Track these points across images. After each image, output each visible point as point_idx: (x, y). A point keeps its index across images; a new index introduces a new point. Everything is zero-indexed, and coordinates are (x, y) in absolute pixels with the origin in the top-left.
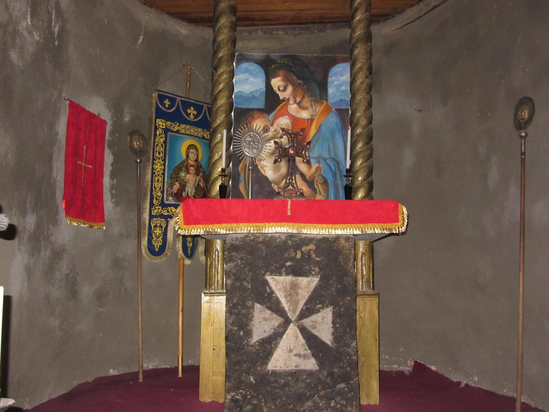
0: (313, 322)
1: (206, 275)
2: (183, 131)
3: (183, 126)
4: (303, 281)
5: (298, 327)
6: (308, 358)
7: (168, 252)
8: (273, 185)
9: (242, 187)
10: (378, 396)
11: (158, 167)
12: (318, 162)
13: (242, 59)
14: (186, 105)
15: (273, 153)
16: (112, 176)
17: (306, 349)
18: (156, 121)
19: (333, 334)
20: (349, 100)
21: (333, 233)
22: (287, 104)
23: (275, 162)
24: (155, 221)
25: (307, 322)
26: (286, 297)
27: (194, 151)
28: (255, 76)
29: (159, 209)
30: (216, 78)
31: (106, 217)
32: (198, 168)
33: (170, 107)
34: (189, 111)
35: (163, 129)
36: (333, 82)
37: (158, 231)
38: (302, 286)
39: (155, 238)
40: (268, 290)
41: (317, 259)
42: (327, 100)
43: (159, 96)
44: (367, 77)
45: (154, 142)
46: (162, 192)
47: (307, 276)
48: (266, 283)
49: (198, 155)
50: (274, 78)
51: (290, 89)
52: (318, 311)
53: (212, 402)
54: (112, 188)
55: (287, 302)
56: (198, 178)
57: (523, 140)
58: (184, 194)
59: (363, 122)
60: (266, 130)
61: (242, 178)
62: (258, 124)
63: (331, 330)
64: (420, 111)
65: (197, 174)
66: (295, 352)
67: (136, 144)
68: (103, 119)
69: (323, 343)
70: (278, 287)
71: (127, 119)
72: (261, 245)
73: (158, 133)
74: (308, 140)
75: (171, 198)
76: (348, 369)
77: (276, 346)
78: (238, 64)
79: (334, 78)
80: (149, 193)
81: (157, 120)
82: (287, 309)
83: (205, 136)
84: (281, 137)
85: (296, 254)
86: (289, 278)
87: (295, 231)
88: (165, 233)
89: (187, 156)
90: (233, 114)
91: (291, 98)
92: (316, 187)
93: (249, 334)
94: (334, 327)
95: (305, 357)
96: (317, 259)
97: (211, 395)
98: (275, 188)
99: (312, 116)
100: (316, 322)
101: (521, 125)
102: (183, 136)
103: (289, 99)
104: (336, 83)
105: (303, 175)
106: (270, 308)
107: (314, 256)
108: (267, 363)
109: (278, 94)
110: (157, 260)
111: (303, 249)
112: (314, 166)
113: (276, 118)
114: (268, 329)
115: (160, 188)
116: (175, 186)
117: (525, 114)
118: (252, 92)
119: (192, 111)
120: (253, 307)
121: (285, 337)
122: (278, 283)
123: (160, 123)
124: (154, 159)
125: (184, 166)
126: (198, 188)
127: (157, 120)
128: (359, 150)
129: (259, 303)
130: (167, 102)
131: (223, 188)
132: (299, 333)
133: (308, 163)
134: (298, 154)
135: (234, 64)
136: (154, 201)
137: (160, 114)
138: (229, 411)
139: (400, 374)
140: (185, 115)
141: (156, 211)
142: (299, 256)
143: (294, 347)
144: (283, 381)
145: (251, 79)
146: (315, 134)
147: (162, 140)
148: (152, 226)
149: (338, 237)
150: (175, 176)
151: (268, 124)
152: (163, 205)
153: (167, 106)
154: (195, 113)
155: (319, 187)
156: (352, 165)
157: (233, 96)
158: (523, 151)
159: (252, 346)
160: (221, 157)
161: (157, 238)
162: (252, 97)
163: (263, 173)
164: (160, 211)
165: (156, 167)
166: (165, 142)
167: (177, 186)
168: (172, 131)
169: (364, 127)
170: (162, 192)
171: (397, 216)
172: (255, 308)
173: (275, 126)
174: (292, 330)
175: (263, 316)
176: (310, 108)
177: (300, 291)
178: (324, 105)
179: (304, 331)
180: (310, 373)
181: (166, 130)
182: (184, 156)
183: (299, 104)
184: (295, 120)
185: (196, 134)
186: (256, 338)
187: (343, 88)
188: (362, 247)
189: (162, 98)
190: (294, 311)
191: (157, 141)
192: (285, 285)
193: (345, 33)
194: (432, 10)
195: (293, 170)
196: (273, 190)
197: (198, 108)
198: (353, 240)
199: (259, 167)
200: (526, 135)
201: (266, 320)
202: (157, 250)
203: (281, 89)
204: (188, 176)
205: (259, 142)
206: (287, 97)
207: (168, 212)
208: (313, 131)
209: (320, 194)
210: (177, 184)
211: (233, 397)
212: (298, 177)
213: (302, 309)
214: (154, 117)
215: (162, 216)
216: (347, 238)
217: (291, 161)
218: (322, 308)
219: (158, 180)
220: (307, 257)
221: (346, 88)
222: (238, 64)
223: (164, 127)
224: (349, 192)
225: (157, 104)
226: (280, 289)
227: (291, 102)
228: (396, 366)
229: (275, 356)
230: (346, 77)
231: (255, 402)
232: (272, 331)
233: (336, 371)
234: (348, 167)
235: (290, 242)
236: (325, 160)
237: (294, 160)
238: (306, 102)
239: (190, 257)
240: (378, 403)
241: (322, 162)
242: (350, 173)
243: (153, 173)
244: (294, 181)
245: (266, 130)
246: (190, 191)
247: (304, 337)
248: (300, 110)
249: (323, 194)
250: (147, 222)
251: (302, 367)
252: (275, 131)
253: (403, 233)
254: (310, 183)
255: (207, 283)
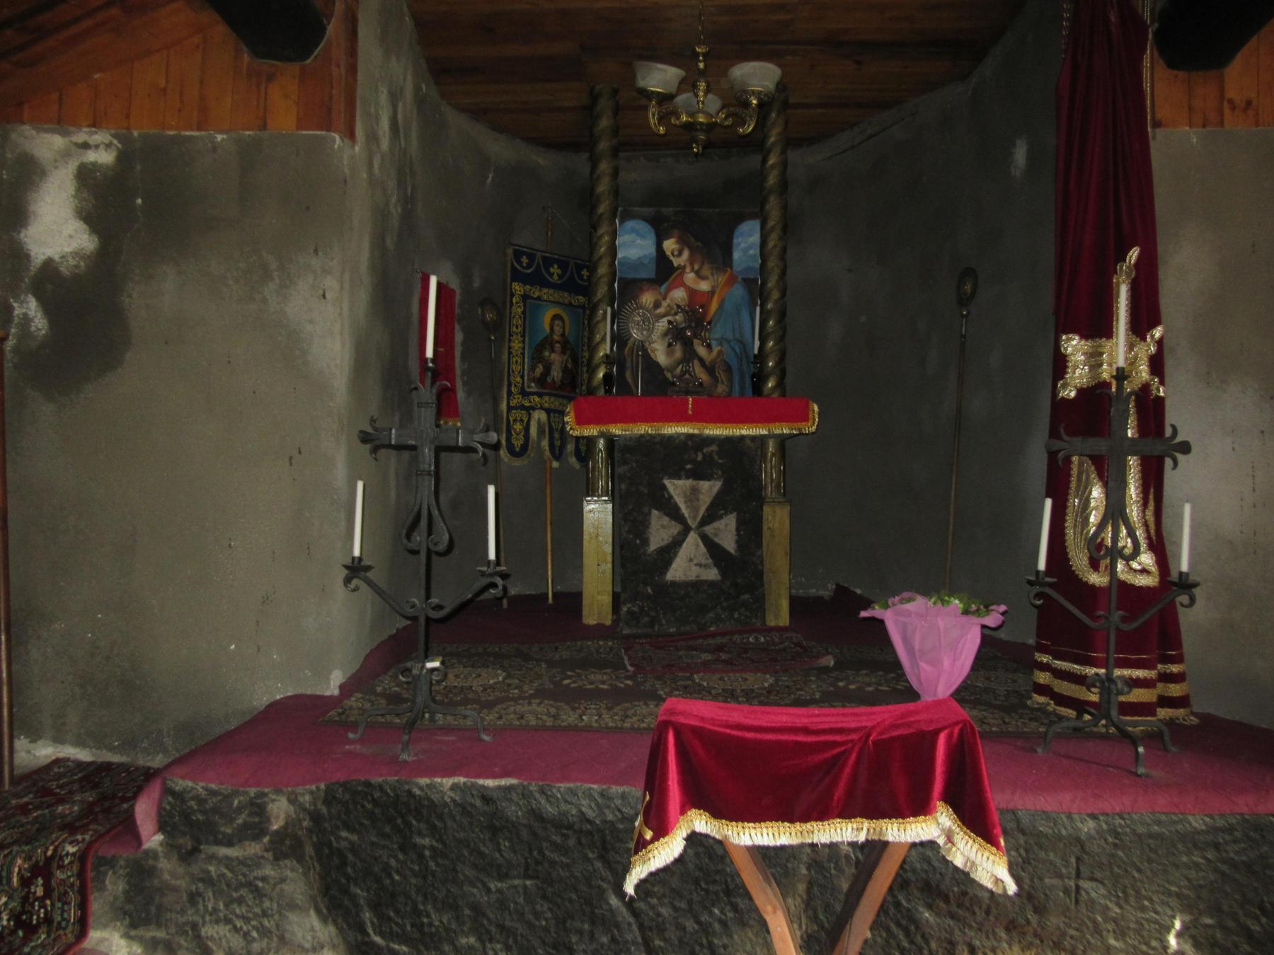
0: (715, 529)
1: (588, 479)
2: (545, 297)
3: (545, 290)
4: (704, 485)
5: (699, 535)
6: (710, 568)
7: (531, 453)
8: (665, 372)
9: (628, 375)
10: (787, 616)
11: (516, 345)
12: (721, 344)
13: (627, 216)
14: (548, 262)
15: (665, 334)
16: (463, 358)
17: (707, 558)
18: (511, 285)
19: (737, 542)
20: (758, 266)
21: (738, 434)
22: (682, 274)
23: (670, 345)
24: (516, 414)
25: (708, 529)
26: (685, 502)
27: (560, 323)
28: (643, 237)
29: (518, 398)
30: (595, 240)
31: (461, 408)
32: (565, 344)
33: (529, 266)
34: (552, 270)
35: (521, 295)
36: (739, 244)
37: (518, 427)
38: (703, 491)
39: (514, 435)
40: (666, 496)
41: (720, 461)
42: (731, 268)
43: (515, 251)
44: (780, 239)
45: (511, 313)
46: (522, 377)
47: (709, 480)
48: (664, 488)
49: (564, 328)
50: (667, 239)
51: (686, 254)
52: (720, 517)
53: (598, 624)
54: (463, 374)
55: (687, 507)
56: (565, 357)
57: (964, 320)
58: (549, 380)
59: (775, 295)
60: (657, 305)
61: (628, 364)
62: (647, 298)
63: (735, 538)
64: (850, 271)
65: (563, 352)
66: (695, 562)
67: (489, 316)
68: (452, 287)
69: (724, 551)
70: (677, 492)
71: (477, 284)
72: (658, 447)
73: (514, 300)
74: (708, 320)
75: (533, 385)
76: (753, 579)
77: (675, 555)
78: (622, 222)
79: (740, 239)
80: (506, 378)
81: (513, 284)
82: (686, 515)
83: (573, 302)
84: (676, 314)
85: (697, 456)
86: (688, 483)
87: (696, 432)
88: (527, 429)
89: (552, 329)
90: (616, 285)
91: (688, 264)
92: (717, 374)
93: (646, 542)
94: (738, 534)
95: (706, 566)
96: (720, 461)
97: (596, 617)
98: (669, 375)
99: (713, 287)
100: (718, 529)
101: (964, 301)
102: (544, 303)
103: (684, 267)
104: (743, 245)
105: (701, 360)
106: (667, 515)
107: (716, 457)
108: (665, 574)
109: (671, 261)
110: (517, 463)
111: (705, 450)
112: (716, 349)
113: (669, 290)
114: (666, 538)
115: (519, 372)
116: (538, 370)
117: (968, 288)
118: (639, 258)
119: (555, 270)
120: (649, 513)
121: (684, 545)
122: (676, 487)
123: (517, 288)
124: (511, 335)
125: (547, 343)
126: (565, 370)
127: (513, 284)
128: (770, 330)
129: (657, 509)
130: (525, 260)
131: (607, 377)
132: (700, 541)
133: (709, 347)
134: (695, 335)
135: (617, 221)
136: (513, 389)
137: (517, 276)
138: (415, 953)
139: (819, 599)
140: (548, 277)
141: (515, 401)
142: (700, 457)
143: (695, 556)
144: (682, 592)
145: (639, 241)
146: (717, 310)
147: (520, 310)
148: (511, 419)
149: (742, 438)
150: (537, 357)
151: (660, 297)
152: (524, 393)
153: (525, 265)
154: (559, 271)
155: (721, 374)
156: (761, 348)
157: (616, 263)
158: (77, 824)
159: (649, 555)
160: (604, 339)
161: (517, 435)
162: (638, 265)
163: (654, 358)
164: (520, 401)
165: (513, 344)
166: (524, 312)
167: (540, 369)
168: (533, 298)
169: (776, 302)
170: (522, 377)
171: (807, 414)
172: (653, 515)
173: (668, 300)
174: (692, 538)
175: (661, 523)
176: (711, 278)
177: (701, 497)
178: (728, 274)
179: (705, 539)
180: (712, 584)
181: (525, 297)
182: (548, 330)
183: (697, 273)
184: (692, 293)
185: (561, 300)
186: (653, 546)
187: (751, 252)
188: (771, 447)
189: (518, 255)
190: (694, 518)
191: (513, 311)
192: (684, 489)
193: (754, 161)
194: (868, 139)
195: (690, 355)
196: (666, 379)
197: (563, 265)
198: (761, 440)
199: (649, 351)
200: (968, 314)
201: (663, 527)
202: (517, 449)
203: (676, 253)
204: (553, 355)
205: (649, 322)
206: (682, 264)
207: (530, 402)
208: (714, 306)
209: (723, 383)
210: (541, 366)
211: (629, 609)
212: (696, 362)
213: (703, 516)
214: (509, 280)
215: (523, 407)
216: (753, 438)
217: (688, 345)
218: (726, 514)
219: (517, 362)
220: (708, 459)
221: (755, 251)
222: (622, 222)
223: (522, 293)
224: (757, 389)
225: (512, 264)
226: (679, 495)
227: (688, 270)
228: (814, 590)
229: (674, 565)
230: (755, 238)
231: (653, 614)
232: (671, 539)
233: (739, 581)
234: (756, 352)
235: (690, 443)
236: (729, 342)
237: (692, 344)
238: (706, 271)
239: (557, 458)
240: (787, 623)
241: (726, 345)
242: (761, 357)
243: (510, 353)
244: (691, 369)
245: (657, 305)
246: (555, 374)
247: (705, 545)
248: (698, 280)
249: (725, 383)
250: (505, 415)
251: (704, 577)
252: (669, 306)
253: (813, 433)
254: (710, 370)
255: (590, 491)
